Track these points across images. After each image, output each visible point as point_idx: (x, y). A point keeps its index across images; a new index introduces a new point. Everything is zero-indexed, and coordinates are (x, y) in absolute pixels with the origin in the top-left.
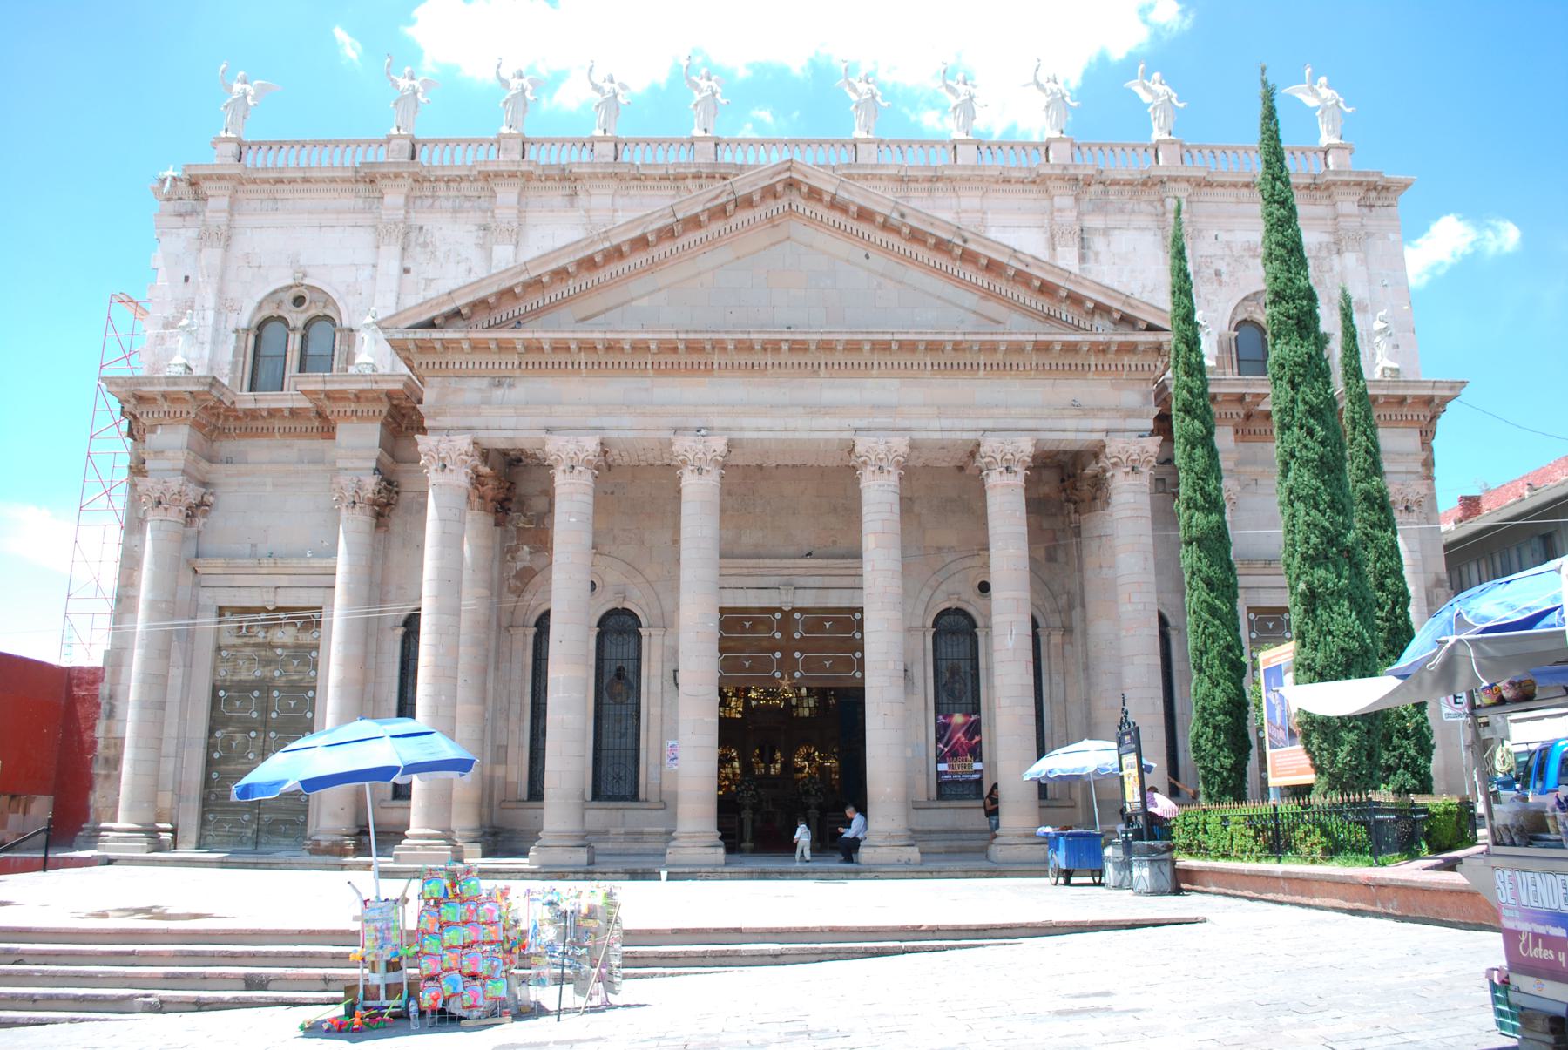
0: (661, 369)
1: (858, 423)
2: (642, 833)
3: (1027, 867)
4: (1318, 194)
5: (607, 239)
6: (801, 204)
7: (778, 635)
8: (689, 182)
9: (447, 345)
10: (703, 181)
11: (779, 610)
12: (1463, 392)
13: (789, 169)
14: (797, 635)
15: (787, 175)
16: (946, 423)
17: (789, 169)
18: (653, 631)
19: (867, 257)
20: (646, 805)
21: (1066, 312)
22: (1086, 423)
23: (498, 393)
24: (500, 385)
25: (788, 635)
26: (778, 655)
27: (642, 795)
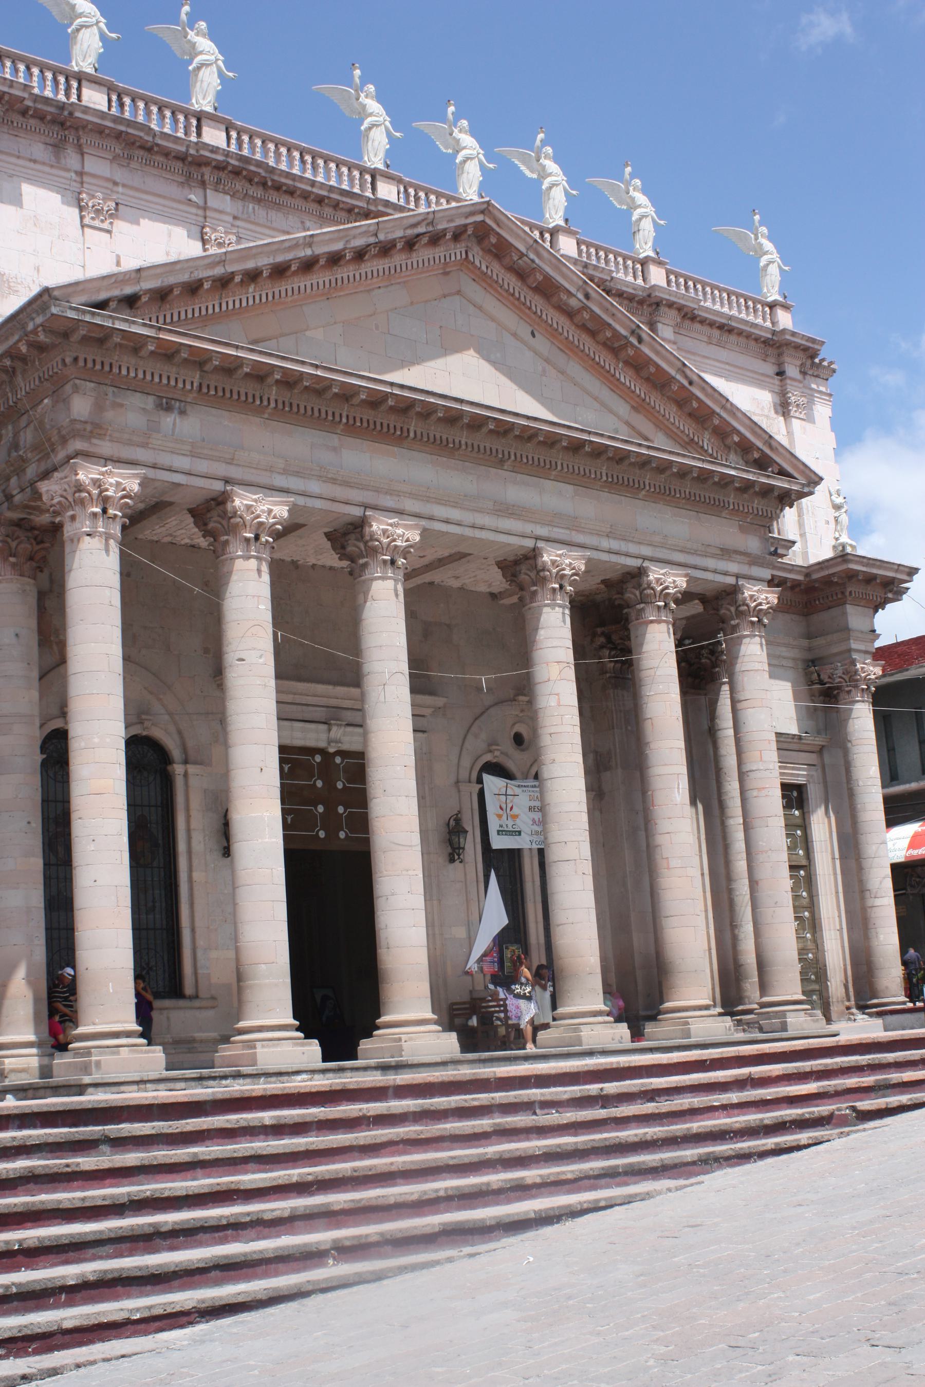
0: (354, 429)
1: (542, 531)
2: (193, 1040)
3: (112, 1129)
4: (770, 351)
5: (310, 245)
6: (478, 257)
7: (319, 784)
8: (207, 171)
9: (135, 344)
10: (223, 175)
11: (322, 751)
12: (915, 577)
13: (482, 212)
14: (340, 785)
15: (479, 218)
16: (615, 545)
17: (482, 212)
18: (192, 769)
19: (533, 335)
20: (196, 1003)
21: (707, 441)
22: (723, 565)
23: (168, 420)
24: (168, 409)
25: (330, 785)
26: (321, 809)
27: (189, 989)
